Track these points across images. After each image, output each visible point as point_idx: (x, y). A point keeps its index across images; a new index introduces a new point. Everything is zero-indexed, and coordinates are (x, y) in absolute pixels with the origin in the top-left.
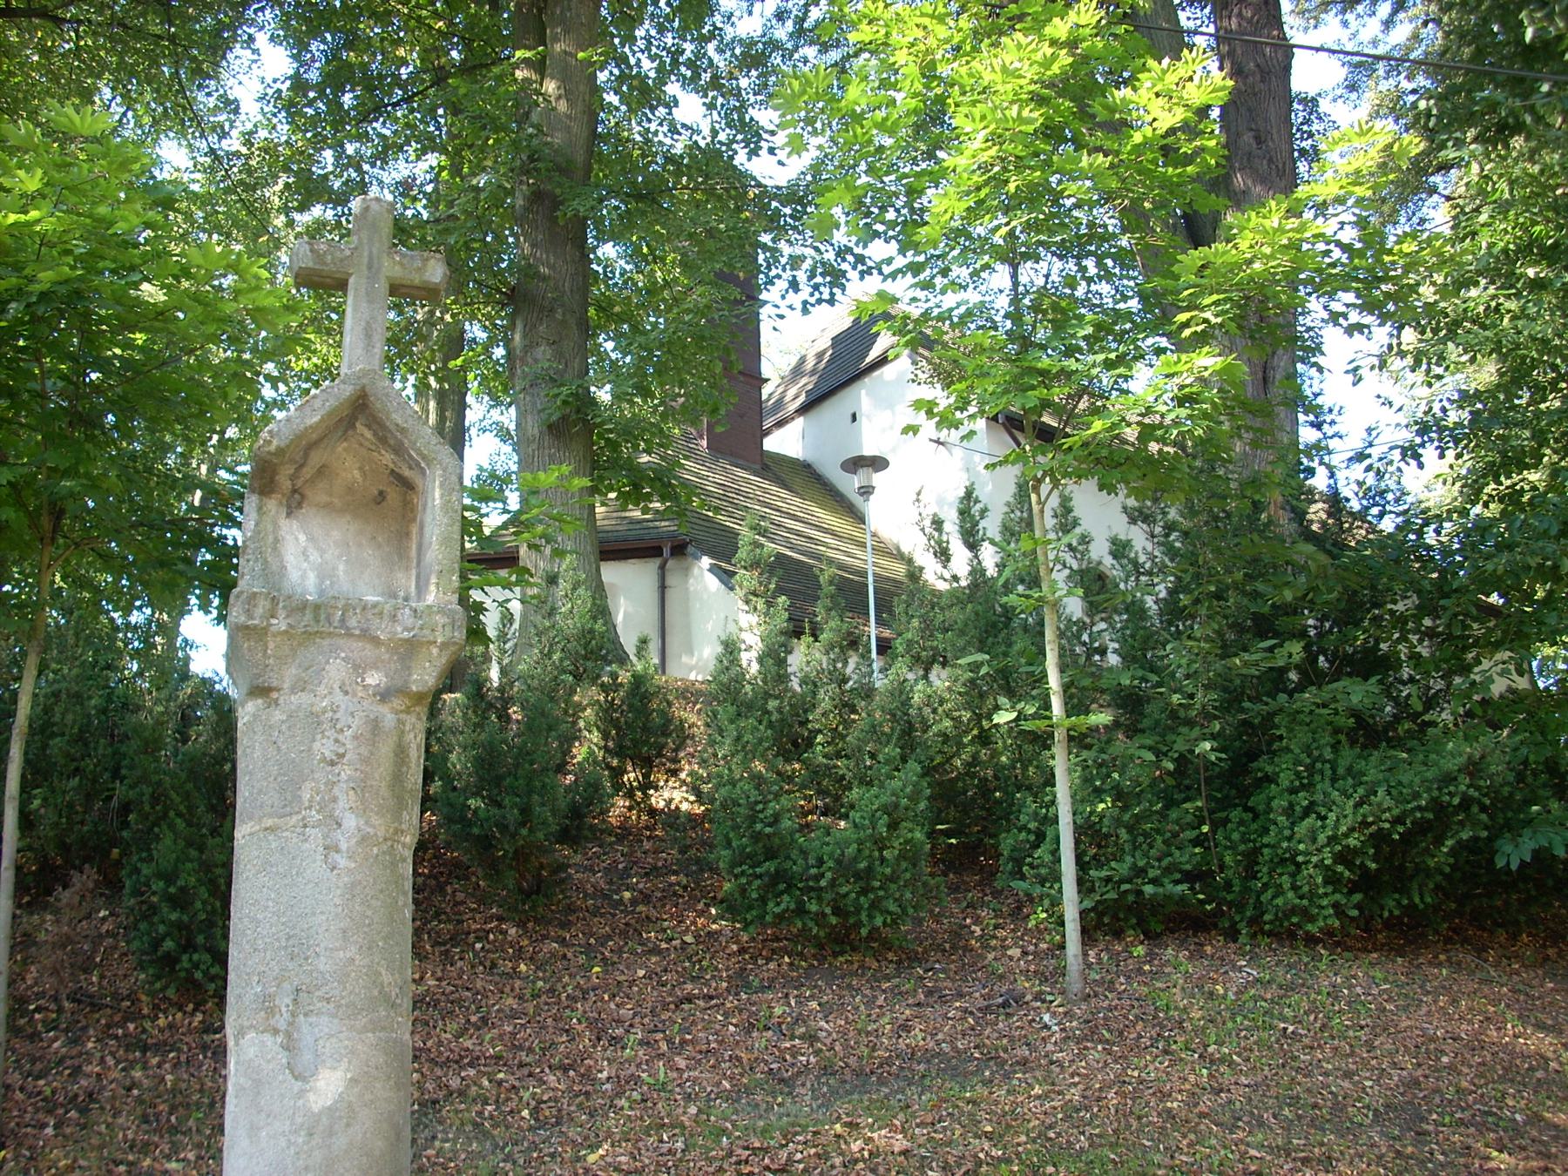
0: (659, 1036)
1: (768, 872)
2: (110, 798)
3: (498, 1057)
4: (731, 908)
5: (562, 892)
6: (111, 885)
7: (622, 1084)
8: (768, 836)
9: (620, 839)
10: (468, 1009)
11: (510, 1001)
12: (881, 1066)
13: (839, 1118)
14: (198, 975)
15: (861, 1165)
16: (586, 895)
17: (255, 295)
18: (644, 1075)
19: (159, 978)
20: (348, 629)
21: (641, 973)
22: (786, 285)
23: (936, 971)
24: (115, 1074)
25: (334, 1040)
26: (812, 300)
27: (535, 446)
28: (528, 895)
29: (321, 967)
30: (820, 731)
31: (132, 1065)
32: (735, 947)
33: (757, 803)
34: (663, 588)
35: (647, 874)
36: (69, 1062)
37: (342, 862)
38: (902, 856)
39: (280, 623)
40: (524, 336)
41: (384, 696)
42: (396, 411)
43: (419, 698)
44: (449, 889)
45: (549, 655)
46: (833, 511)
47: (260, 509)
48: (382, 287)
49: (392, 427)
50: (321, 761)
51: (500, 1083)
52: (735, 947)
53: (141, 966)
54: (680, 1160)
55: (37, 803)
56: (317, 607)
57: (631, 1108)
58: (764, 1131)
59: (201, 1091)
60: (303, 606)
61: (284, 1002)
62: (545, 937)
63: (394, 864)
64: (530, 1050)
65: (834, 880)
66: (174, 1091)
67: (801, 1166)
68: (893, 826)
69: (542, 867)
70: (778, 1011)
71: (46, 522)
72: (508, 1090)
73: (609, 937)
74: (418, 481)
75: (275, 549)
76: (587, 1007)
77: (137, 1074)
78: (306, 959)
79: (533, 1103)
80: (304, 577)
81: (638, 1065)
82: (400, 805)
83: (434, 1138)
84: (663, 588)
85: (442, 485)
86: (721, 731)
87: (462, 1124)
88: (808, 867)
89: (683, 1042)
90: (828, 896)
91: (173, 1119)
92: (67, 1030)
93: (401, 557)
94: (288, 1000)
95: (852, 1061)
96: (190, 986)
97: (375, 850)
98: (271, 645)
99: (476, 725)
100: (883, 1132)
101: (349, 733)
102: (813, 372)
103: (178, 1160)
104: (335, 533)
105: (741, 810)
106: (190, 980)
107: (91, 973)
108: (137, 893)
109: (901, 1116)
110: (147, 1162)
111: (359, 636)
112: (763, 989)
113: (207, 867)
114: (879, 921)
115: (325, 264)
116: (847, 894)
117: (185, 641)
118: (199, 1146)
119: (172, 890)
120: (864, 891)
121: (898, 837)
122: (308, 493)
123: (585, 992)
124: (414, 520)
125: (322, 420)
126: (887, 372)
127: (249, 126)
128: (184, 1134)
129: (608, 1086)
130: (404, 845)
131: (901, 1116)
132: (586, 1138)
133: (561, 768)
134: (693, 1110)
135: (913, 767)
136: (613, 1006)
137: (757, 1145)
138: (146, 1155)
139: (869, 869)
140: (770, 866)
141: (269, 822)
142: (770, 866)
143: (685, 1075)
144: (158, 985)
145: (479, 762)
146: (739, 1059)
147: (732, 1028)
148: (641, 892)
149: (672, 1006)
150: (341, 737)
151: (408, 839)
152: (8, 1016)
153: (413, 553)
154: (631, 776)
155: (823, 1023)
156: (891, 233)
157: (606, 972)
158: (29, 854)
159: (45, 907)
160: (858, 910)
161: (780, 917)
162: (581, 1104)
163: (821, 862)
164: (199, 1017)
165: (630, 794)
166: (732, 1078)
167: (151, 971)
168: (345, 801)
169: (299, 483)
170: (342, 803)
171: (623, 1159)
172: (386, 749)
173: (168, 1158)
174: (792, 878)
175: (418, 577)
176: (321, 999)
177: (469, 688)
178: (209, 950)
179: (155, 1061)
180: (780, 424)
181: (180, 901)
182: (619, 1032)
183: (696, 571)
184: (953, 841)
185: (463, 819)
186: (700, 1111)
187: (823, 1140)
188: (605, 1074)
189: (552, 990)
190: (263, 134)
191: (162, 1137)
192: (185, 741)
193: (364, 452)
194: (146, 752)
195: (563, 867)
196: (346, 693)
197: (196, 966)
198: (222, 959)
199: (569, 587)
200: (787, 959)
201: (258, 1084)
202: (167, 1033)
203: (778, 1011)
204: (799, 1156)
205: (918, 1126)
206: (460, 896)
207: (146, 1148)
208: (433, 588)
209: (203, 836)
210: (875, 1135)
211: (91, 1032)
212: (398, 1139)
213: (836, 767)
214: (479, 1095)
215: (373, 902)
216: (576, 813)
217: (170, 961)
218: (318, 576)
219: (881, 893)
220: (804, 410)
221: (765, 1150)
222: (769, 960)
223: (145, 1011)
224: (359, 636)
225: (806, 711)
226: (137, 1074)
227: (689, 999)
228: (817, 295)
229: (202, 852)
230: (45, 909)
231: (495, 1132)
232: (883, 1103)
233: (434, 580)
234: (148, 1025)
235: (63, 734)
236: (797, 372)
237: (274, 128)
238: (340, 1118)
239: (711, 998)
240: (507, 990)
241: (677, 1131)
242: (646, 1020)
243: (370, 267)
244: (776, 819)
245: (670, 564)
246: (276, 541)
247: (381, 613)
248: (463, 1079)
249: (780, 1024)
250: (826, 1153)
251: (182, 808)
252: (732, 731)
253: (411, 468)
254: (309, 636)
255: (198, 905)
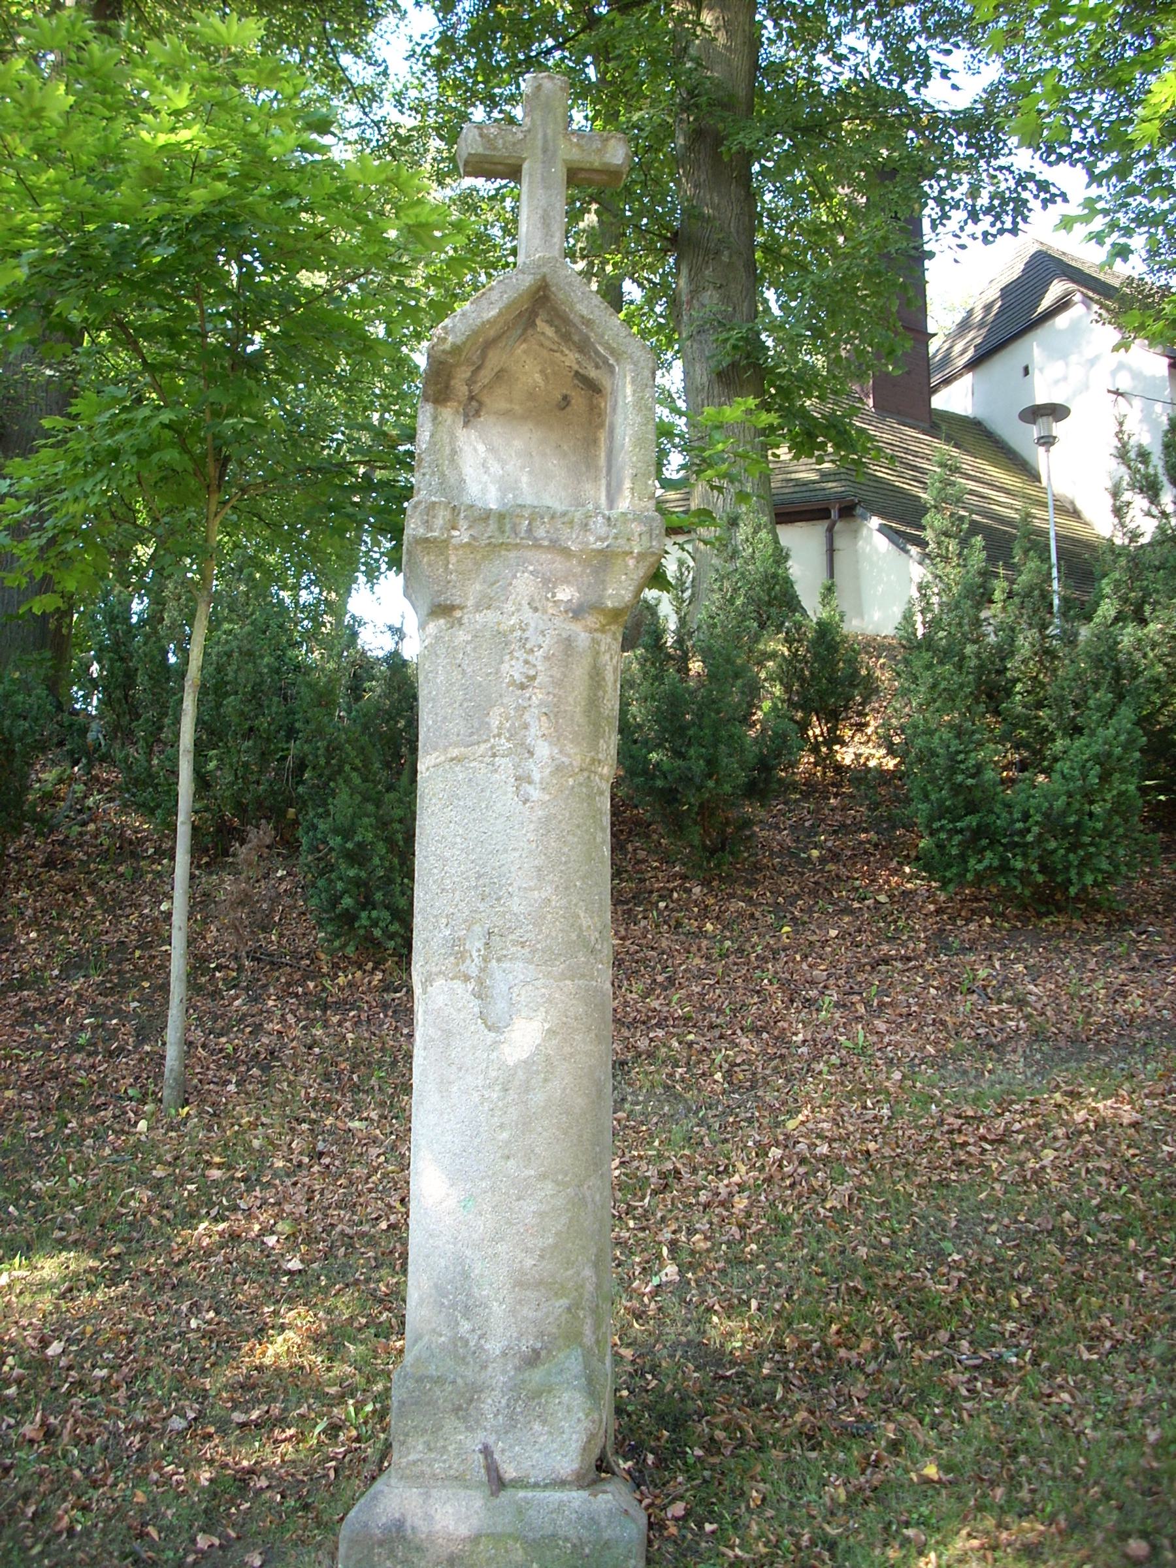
0: (856, 998)
1: (969, 827)
2: (284, 758)
3: (687, 1019)
4: (928, 864)
5: (747, 849)
6: (287, 844)
7: (819, 1048)
8: (970, 788)
9: (806, 796)
10: (654, 968)
11: (697, 961)
12: (1097, 1033)
13: (1058, 1086)
14: (377, 933)
15: (1086, 1137)
16: (772, 853)
17: (417, 210)
18: (843, 1039)
19: (338, 936)
20: (536, 539)
21: (833, 933)
22: (965, 215)
23: (1150, 934)
24: (297, 1032)
25: (530, 987)
26: (994, 231)
27: (704, 395)
28: (713, 852)
29: (515, 909)
30: (1019, 680)
31: (313, 1022)
32: (932, 907)
33: (958, 752)
34: (831, 551)
35: (835, 832)
36: (250, 1020)
37: (535, 793)
38: (1114, 811)
39: (462, 535)
40: (691, 280)
41: (577, 612)
42: (582, 301)
43: (615, 615)
44: (630, 847)
45: (731, 601)
46: (1007, 469)
47: (435, 418)
48: (559, 173)
49: (577, 320)
50: (510, 684)
51: (690, 1045)
52: (932, 907)
53: (320, 925)
54: (887, 1128)
55: (212, 765)
56: (501, 517)
57: (829, 1073)
58: (976, 1100)
59: (382, 1050)
60: (486, 516)
61: (475, 945)
62: (732, 896)
63: (590, 797)
64: (720, 1011)
65: (1040, 834)
66: (355, 1050)
67: (1021, 1137)
68: (1105, 777)
69: (727, 823)
70: (982, 973)
71: (212, 469)
72: (700, 1053)
73: (798, 896)
74: (606, 383)
75: (452, 461)
76: (779, 967)
77: (318, 1032)
78: (498, 899)
79: (726, 1066)
80: (484, 491)
81: (836, 1028)
82: (596, 734)
83: (624, 1100)
84: (831, 551)
85: (633, 381)
86: (915, 679)
87: (653, 1087)
88: (1013, 822)
89: (882, 1005)
90: (1036, 852)
91: (355, 1077)
92: (247, 989)
93: (588, 467)
94: (479, 944)
95: (1066, 1027)
96: (369, 945)
97: (571, 781)
98: (453, 559)
99: (656, 678)
100: (1109, 1102)
101: (539, 654)
102: (981, 325)
103: (361, 1120)
104: (516, 443)
105: (941, 761)
106: (369, 938)
107: (270, 932)
108: (314, 849)
109: (1126, 1086)
110: (329, 1121)
111: (548, 547)
112: (964, 951)
113: (383, 824)
114: (1089, 879)
115: (495, 149)
116: (1054, 851)
117: (353, 617)
118: (382, 1104)
119: (349, 845)
120: (1073, 848)
121: (1110, 790)
122: (486, 400)
123: (775, 952)
124: (602, 425)
125: (500, 314)
126: (1061, 321)
127: (399, 87)
128: (367, 1092)
129: (804, 1050)
130: (601, 777)
131: (1126, 1086)
132: (785, 1103)
133: (746, 720)
134: (897, 1076)
135: (1126, 714)
136: (805, 966)
137: (970, 1113)
138: (328, 1113)
139: (1078, 825)
140: (972, 821)
141: (454, 752)
142: (972, 821)
143: (886, 1040)
144: (337, 944)
145: (659, 717)
146: (943, 1023)
147: (933, 991)
148: (829, 850)
149: (868, 968)
150: (531, 658)
151: (606, 770)
152: (188, 975)
153: (602, 461)
154: (816, 730)
155: (1031, 987)
156: (1076, 156)
157: (797, 932)
158: (207, 815)
159: (224, 866)
160: (1067, 869)
161: (980, 878)
162: (775, 1068)
163: (1026, 817)
164: (379, 976)
165: (815, 750)
166: (936, 1043)
167: (330, 929)
168: (537, 730)
169: (476, 388)
170: (533, 731)
171: (825, 1125)
172: (580, 671)
173: (351, 1116)
174: (994, 833)
175: (609, 485)
176: (515, 943)
177: (646, 639)
178: (387, 908)
179: (335, 1019)
180: (947, 382)
181: (357, 857)
182: (813, 993)
183: (865, 532)
184: (1162, 798)
185: (645, 772)
186: (904, 1077)
187: (1042, 1109)
188: (800, 1037)
189: (741, 950)
190: (413, 93)
191: (344, 1095)
192: (358, 698)
193: (545, 353)
194: (320, 705)
195: (747, 823)
196: (536, 610)
197: (375, 924)
198: (404, 917)
199: (750, 530)
200: (988, 920)
201: (448, 1034)
202: (347, 992)
203: (982, 973)
204: (1017, 1126)
205: (1147, 1096)
206: (642, 854)
207: (329, 1106)
208: (627, 493)
209: (380, 792)
210: (1100, 1106)
211: (272, 990)
212: (599, 1097)
213: (1037, 717)
214: (669, 1057)
215: (570, 838)
216: (765, 766)
217: (349, 919)
218: (500, 489)
219: (1092, 849)
220: (972, 365)
221: (980, 1119)
222: (968, 921)
223: (325, 970)
224: (548, 547)
225: (1003, 659)
226: (318, 1032)
227: (886, 961)
228: (998, 225)
229: (378, 807)
230: (223, 868)
231: (688, 1096)
232: (1105, 1071)
233: (627, 484)
234: (327, 983)
235: (236, 693)
236: (964, 326)
237: (423, 86)
238: (538, 1072)
239: (909, 959)
240: (694, 949)
241: (881, 1097)
242: (841, 982)
243: (545, 151)
244: (979, 769)
245: (838, 526)
246: (454, 452)
247: (572, 522)
248: (651, 1040)
249: (985, 987)
250: (1047, 1123)
251: (357, 761)
252: (927, 678)
253: (597, 367)
254: (494, 548)
255: (376, 861)
